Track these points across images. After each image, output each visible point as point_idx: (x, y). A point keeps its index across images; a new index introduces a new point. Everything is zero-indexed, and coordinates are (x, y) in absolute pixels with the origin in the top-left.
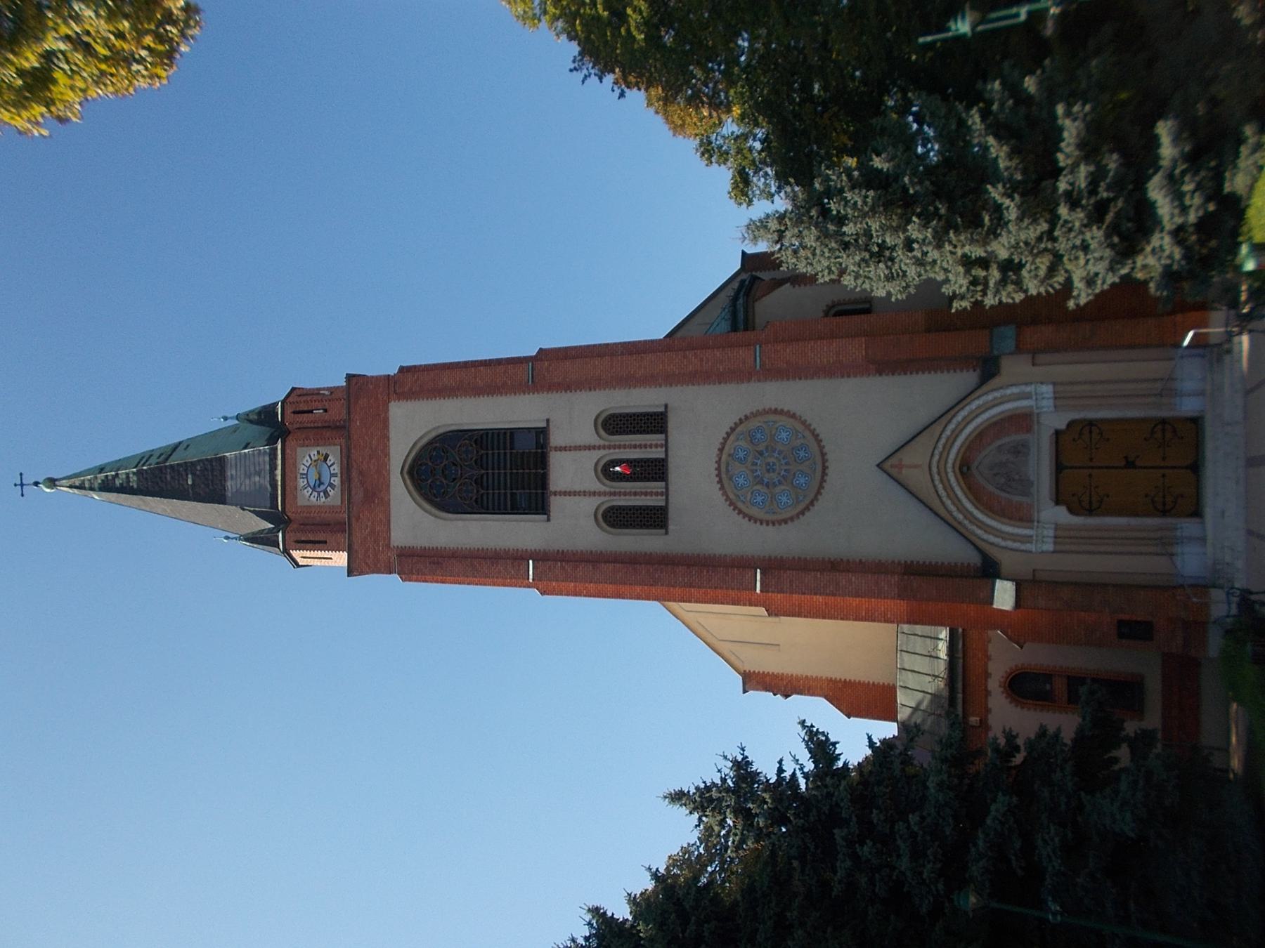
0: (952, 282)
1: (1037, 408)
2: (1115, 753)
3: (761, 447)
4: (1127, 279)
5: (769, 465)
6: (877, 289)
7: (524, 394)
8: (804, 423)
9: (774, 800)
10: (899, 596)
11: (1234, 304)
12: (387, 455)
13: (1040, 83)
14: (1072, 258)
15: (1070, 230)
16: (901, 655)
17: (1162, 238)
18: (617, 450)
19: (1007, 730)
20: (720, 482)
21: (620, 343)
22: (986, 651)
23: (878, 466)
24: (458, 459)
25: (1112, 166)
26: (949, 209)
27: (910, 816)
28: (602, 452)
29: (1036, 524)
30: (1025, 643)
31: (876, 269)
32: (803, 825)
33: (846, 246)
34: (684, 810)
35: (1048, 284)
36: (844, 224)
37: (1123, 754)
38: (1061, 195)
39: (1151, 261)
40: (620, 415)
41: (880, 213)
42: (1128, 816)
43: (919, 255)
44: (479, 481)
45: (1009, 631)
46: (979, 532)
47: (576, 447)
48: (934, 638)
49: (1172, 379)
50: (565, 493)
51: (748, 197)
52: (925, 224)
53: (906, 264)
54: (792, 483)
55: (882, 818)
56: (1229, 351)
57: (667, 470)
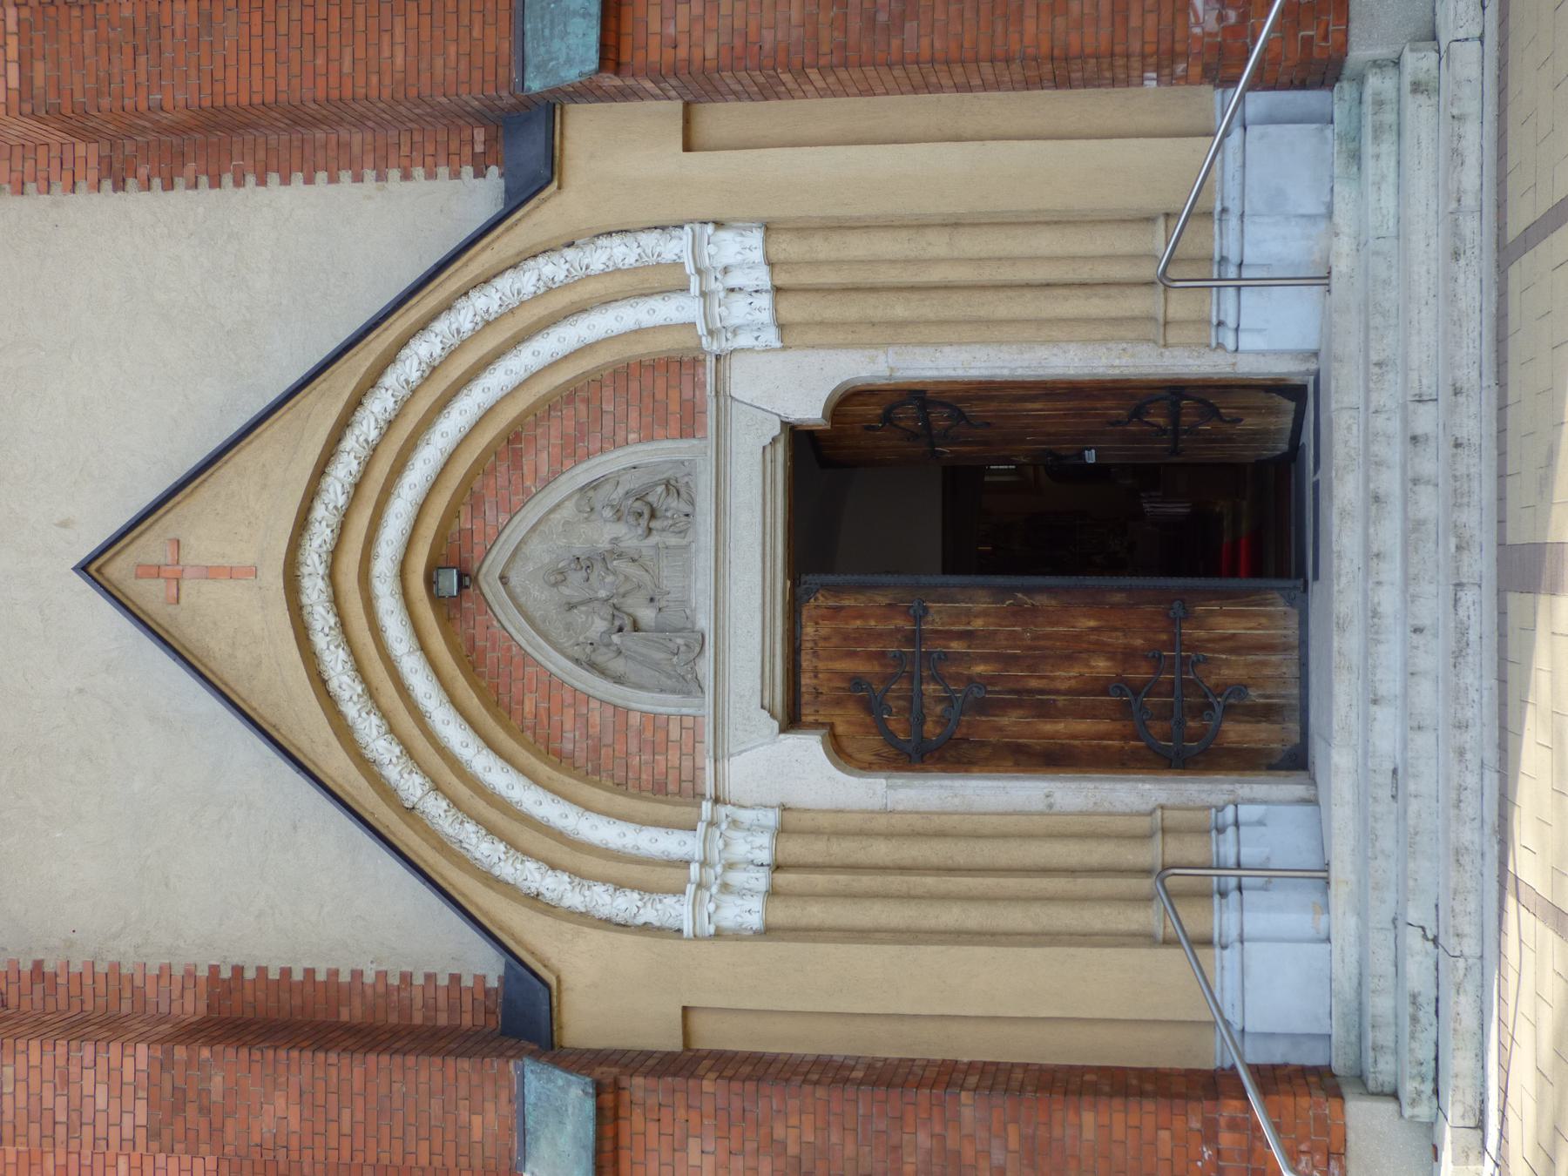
1: (711, 333)
10: (153, 1134)
23: (83, 568)
29: (706, 806)
46: (485, 850)
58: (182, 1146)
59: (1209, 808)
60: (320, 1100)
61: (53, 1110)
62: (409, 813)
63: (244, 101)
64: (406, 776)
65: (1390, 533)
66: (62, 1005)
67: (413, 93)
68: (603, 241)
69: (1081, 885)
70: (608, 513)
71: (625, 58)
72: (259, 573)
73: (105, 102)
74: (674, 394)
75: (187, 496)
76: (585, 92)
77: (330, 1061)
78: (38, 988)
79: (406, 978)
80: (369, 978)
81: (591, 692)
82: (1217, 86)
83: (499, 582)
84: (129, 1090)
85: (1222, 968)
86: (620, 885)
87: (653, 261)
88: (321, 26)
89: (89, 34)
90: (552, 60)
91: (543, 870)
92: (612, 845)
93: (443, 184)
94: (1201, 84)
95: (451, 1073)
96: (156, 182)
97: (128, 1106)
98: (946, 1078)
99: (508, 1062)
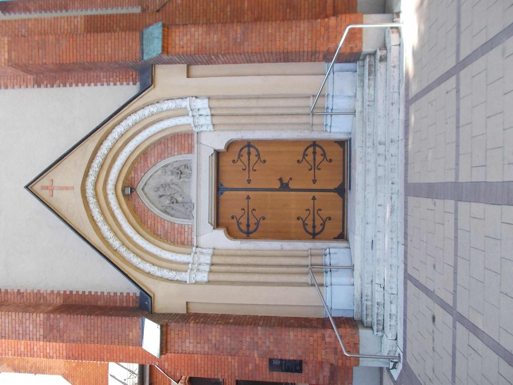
10: (45, 337)
23: (27, 187)
29: (194, 248)
46: (135, 260)
49: (324, 96)
58: (52, 340)
59: (322, 249)
60: (89, 328)
61: (19, 331)
62: (115, 251)
63: (68, 62)
64: (114, 241)
65: (370, 179)
66: (25, 301)
67: (113, 60)
68: (166, 102)
69: (290, 270)
70: (170, 173)
71: (170, 50)
72: (74, 188)
73: (31, 62)
74: (186, 142)
75: (55, 168)
76: (159, 61)
77: (91, 318)
78: (19, 296)
79: (115, 294)
80: (105, 294)
81: (165, 219)
82: (326, 62)
83: (142, 191)
84: (38, 326)
85: (326, 292)
86: (171, 270)
87: (179, 107)
88: (89, 42)
89: (27, 44)
90: (149, 51)
91: (151, 266)
92: (169, 259)
93: (125, 87)
94: (322, 61)
95: (124, 321)
96: (49, 85)
97: (38, 330)
98: (254, 322)
99: (139, 318)
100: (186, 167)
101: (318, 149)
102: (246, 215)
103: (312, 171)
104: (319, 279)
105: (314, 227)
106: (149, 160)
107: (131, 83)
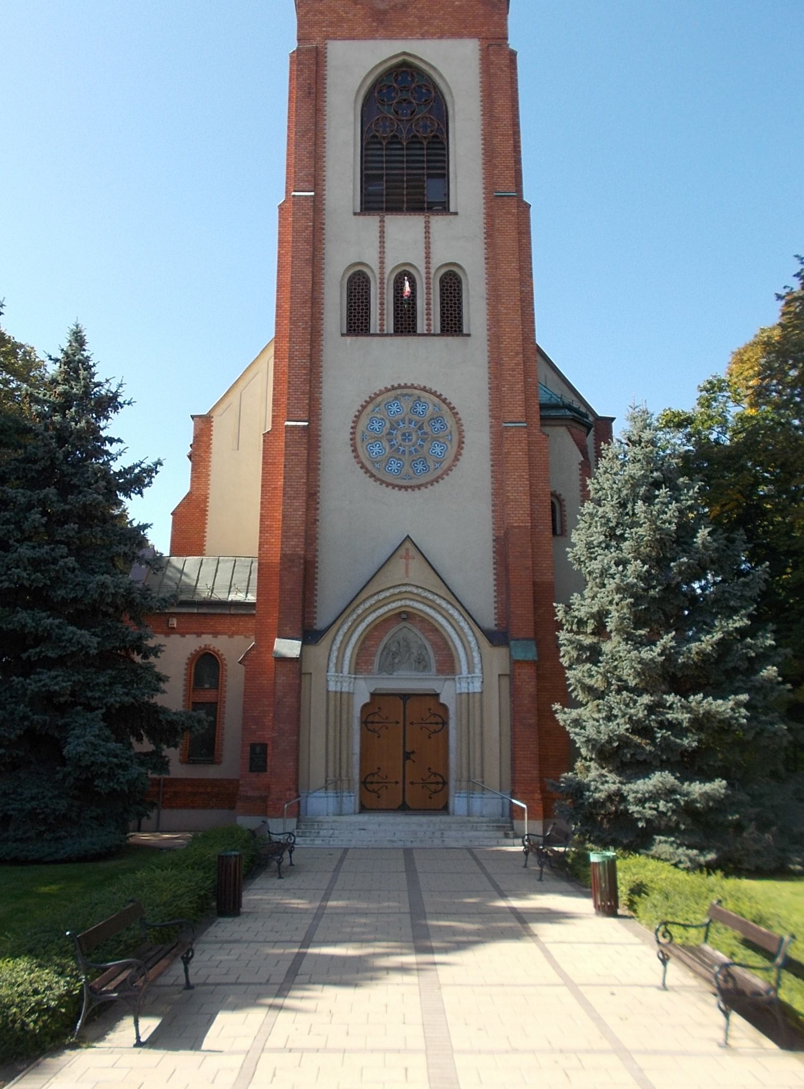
0: (582, 602)
1: (459, 678)
2: (145, 739)
3: (426, 428)
4: (577, 753)
5: (409, 436)
6: (579, 534)
7: (484, 188)
8: (450, 469)
9: (78, 431)
11: (549, 841)
12: (424, 36)
13: (770, 680)
14: (600, 707)
15: (627, 705)
16: (231, 560)
17: (614, 783)
18: (425, 286)
19: (163, 648)
20: (394, 388)
21: (532, 290)
22: (237, 634)
23: (408, 536)
24: (417, 117)
25: (686, 742)
26: (653, 598)
27: (73, 558)
28: (423, 271)
29: (354, 676)
30: (244, 665)
31: (599, 532)
32: (58, 459)
33: (623, 505)
34: (65, 346)
35: (577, 686)
36: (644, 502)
37: (146, 746)
38: (662, 697)
39: (593, 774)
40: (460, 290)
41: (654, 536)
42: (81, 749)
43: (612, 571)
44: (394, 140)
45: (255, 652)
46: (345, 627)
47: (429, 243)
48: (247, 589)
50: (382, 232)
51: (664, 427)
52: (641, 577)
53: (603, 560)
54: (392, 457)
55: (71, 534)
56: (506, 836)
57: (405, 336)
93: (493, 617)
100: (425, 667)
101: (441, 786)
102: (381, 720)
103: (421, 781)
104: (331, 787)
105: (372, 783)
106: (430, 633)
107: (496, 622)
